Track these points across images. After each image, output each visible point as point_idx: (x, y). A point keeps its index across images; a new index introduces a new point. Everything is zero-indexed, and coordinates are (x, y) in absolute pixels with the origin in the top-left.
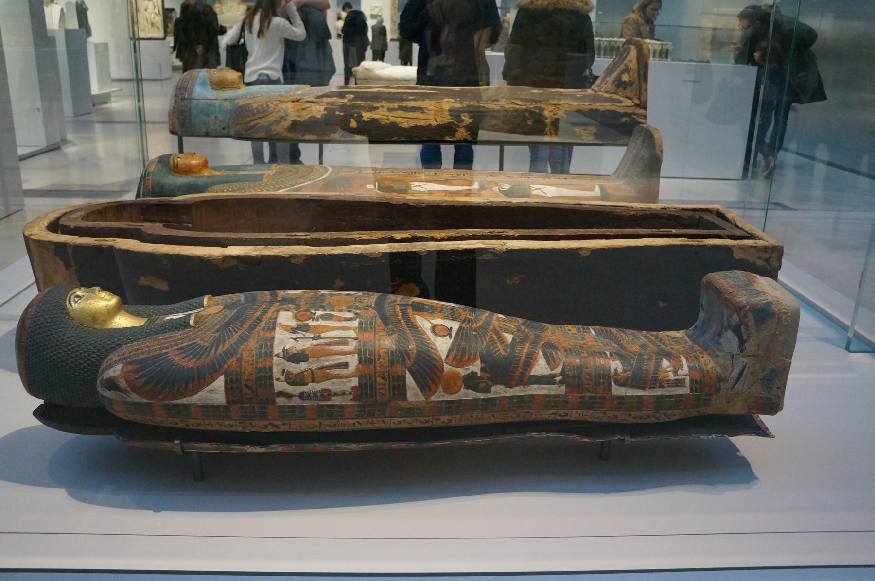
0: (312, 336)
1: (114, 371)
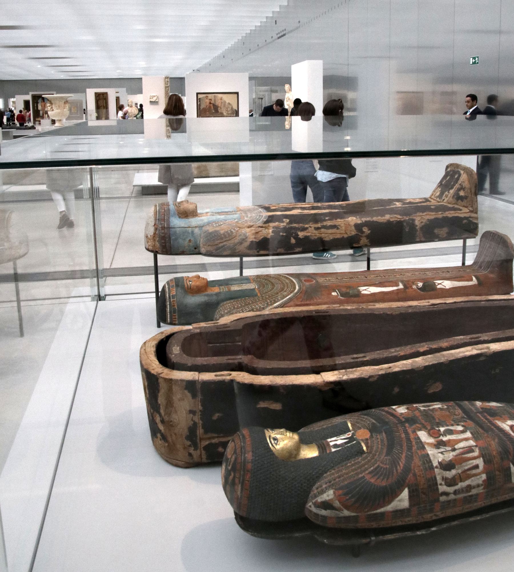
0: (450, 449)
1: (328, 496)
